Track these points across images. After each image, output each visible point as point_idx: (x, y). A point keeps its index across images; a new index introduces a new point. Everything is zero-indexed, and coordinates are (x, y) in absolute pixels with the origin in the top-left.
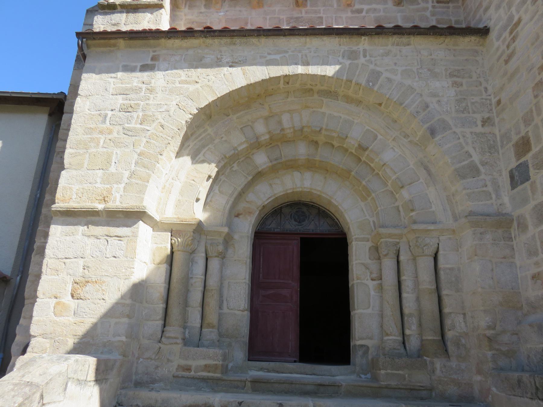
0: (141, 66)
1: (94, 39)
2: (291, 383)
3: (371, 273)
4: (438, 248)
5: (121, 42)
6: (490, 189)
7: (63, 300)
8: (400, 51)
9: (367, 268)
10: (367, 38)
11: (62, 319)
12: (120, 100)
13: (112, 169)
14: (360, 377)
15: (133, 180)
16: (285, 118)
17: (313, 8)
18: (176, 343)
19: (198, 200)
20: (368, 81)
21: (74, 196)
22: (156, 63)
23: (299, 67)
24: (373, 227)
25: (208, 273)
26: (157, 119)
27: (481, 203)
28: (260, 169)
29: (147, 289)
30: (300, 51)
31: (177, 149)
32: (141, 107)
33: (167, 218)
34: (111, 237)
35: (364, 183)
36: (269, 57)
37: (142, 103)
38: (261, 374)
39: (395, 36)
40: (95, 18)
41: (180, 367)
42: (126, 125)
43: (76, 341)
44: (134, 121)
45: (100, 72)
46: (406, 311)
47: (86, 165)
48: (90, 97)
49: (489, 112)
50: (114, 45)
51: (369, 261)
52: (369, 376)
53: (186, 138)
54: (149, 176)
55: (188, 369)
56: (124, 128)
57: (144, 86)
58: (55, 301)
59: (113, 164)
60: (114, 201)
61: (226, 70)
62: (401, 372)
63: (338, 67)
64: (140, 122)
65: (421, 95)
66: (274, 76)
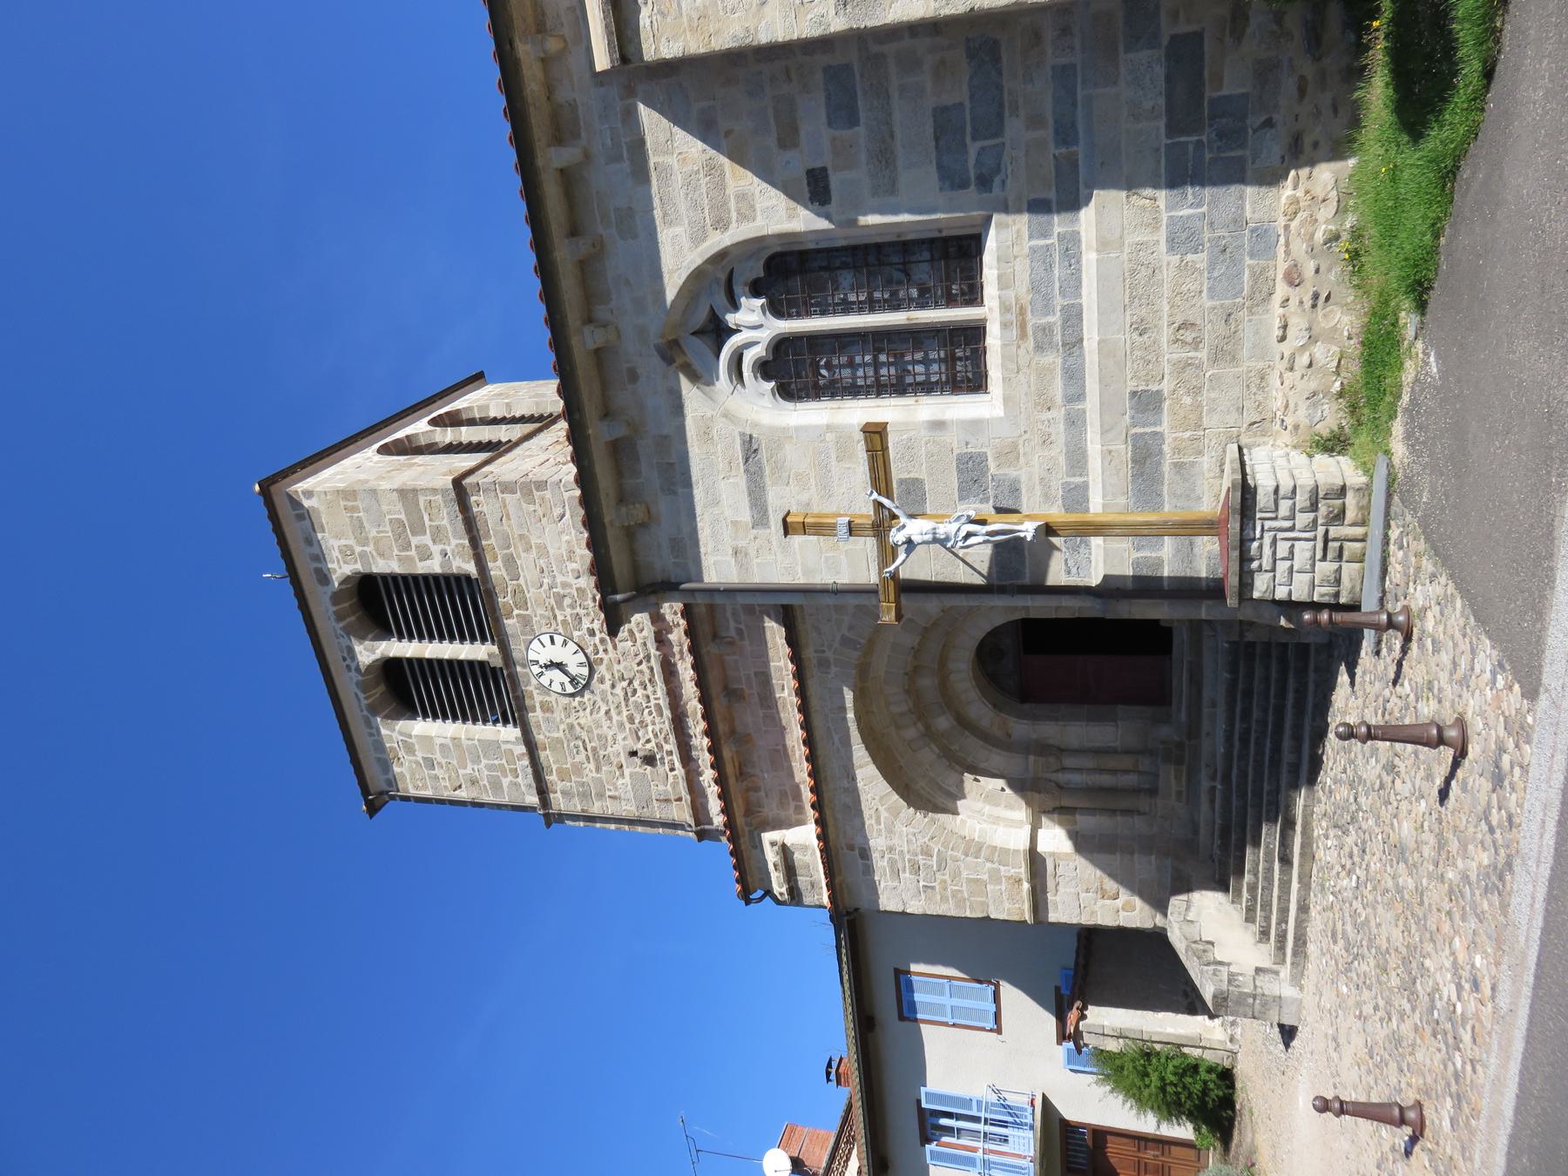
13: (985, 877)
16: (896, 709)
20: (855, 649)
21: (1017, 906)
31: (951, 816)
55: (1179, 793)
58: (1121, 913)
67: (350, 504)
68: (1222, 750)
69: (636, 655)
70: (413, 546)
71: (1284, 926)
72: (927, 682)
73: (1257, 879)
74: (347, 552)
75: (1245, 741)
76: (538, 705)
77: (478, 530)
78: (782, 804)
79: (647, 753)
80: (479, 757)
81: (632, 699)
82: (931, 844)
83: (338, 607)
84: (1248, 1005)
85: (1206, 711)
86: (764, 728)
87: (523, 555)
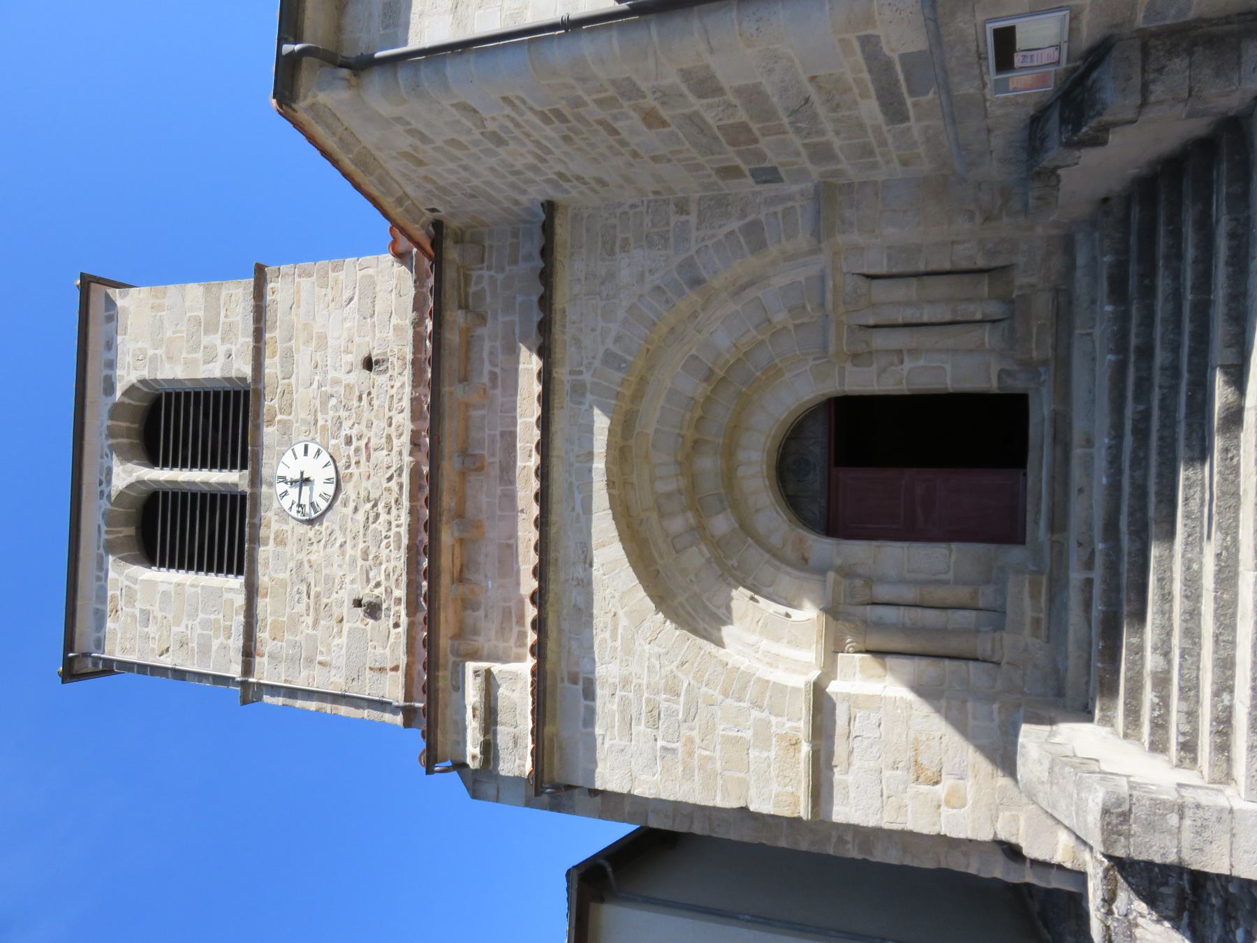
0: (585, 699)
1: (543, 770)
2: (1052, 478)
3: (892, 364)
4: (859, 274)
5: (548, 730)
6: (779, 209)
7: (943, 796)
8: (574, 323)
9: (885, 370)
10: (555, 370)
11: (969, 797)
12: (640, 728)
13: (748, 735)
14: (1044, 381)
15: (765, 703)
16: (663, 487)
17: (486, 446)
18: (1001, 639)
19: (788, 615)
20: (619, 369)
22: (581, 676)
23: (595, 466)
24: (823, 360)
25: (896, 601)
26: (672, 672)
27: (800, 221)
28: (737, 526)
29: (922, 685)
30: (571, 465)
32: (652, 697)
33: (816, 659)
34: (849, 733)
35: (758, 374)
36: (578, 509)
37: (646, 695)
38: (1043, 523)
39: (553, 329)
40: (502, 773)
41: (1035, 634)
42: (680, 716)
43: (1000, 773)
44: (675, 706)
45: (594, 762)
46: (948, 318)
47: (742, 775)
48: (633, 774)
49: (668, 204)
50: (552, 741)
51: (875, 366)
52: (1042, 370)
53: (695, 631)
54: (759, 679)
55: (1036, 622)
56: (685, 721)
57: (618, 693)
58: (943, 808)
59: (740, 734)
60: (797, 729)
61: (597, 572)
62: (1034, 330)
63: (597, 412)
64: (676, 698)
65: (641, 296)
66: (608, 502)
67: (158, 301)
68: (1104, 481)
69: (388, 468)
70: (202, 346)
71: (1226, 696)
72: (707, 463)
73: (1169, 662)
74: (140, 357)
75: (1141, 434)
76: (272, 536)
77: (266, 321)
78: (503, 632)
79: (373, 600)
80: (197, 610)
81: (372, 527)
82: (680, 675)
83: (115, 423)
84: (1169, 832)
85: (1077, 452)
86: (499, 513)
87: (302, 348)
